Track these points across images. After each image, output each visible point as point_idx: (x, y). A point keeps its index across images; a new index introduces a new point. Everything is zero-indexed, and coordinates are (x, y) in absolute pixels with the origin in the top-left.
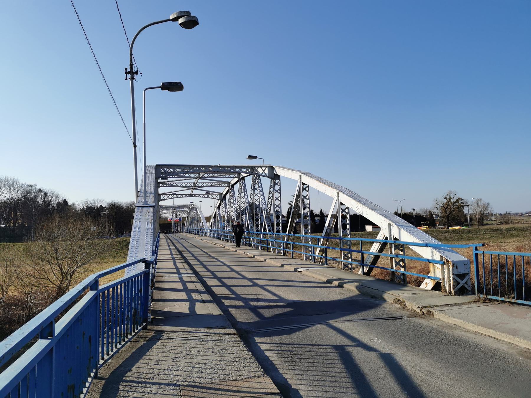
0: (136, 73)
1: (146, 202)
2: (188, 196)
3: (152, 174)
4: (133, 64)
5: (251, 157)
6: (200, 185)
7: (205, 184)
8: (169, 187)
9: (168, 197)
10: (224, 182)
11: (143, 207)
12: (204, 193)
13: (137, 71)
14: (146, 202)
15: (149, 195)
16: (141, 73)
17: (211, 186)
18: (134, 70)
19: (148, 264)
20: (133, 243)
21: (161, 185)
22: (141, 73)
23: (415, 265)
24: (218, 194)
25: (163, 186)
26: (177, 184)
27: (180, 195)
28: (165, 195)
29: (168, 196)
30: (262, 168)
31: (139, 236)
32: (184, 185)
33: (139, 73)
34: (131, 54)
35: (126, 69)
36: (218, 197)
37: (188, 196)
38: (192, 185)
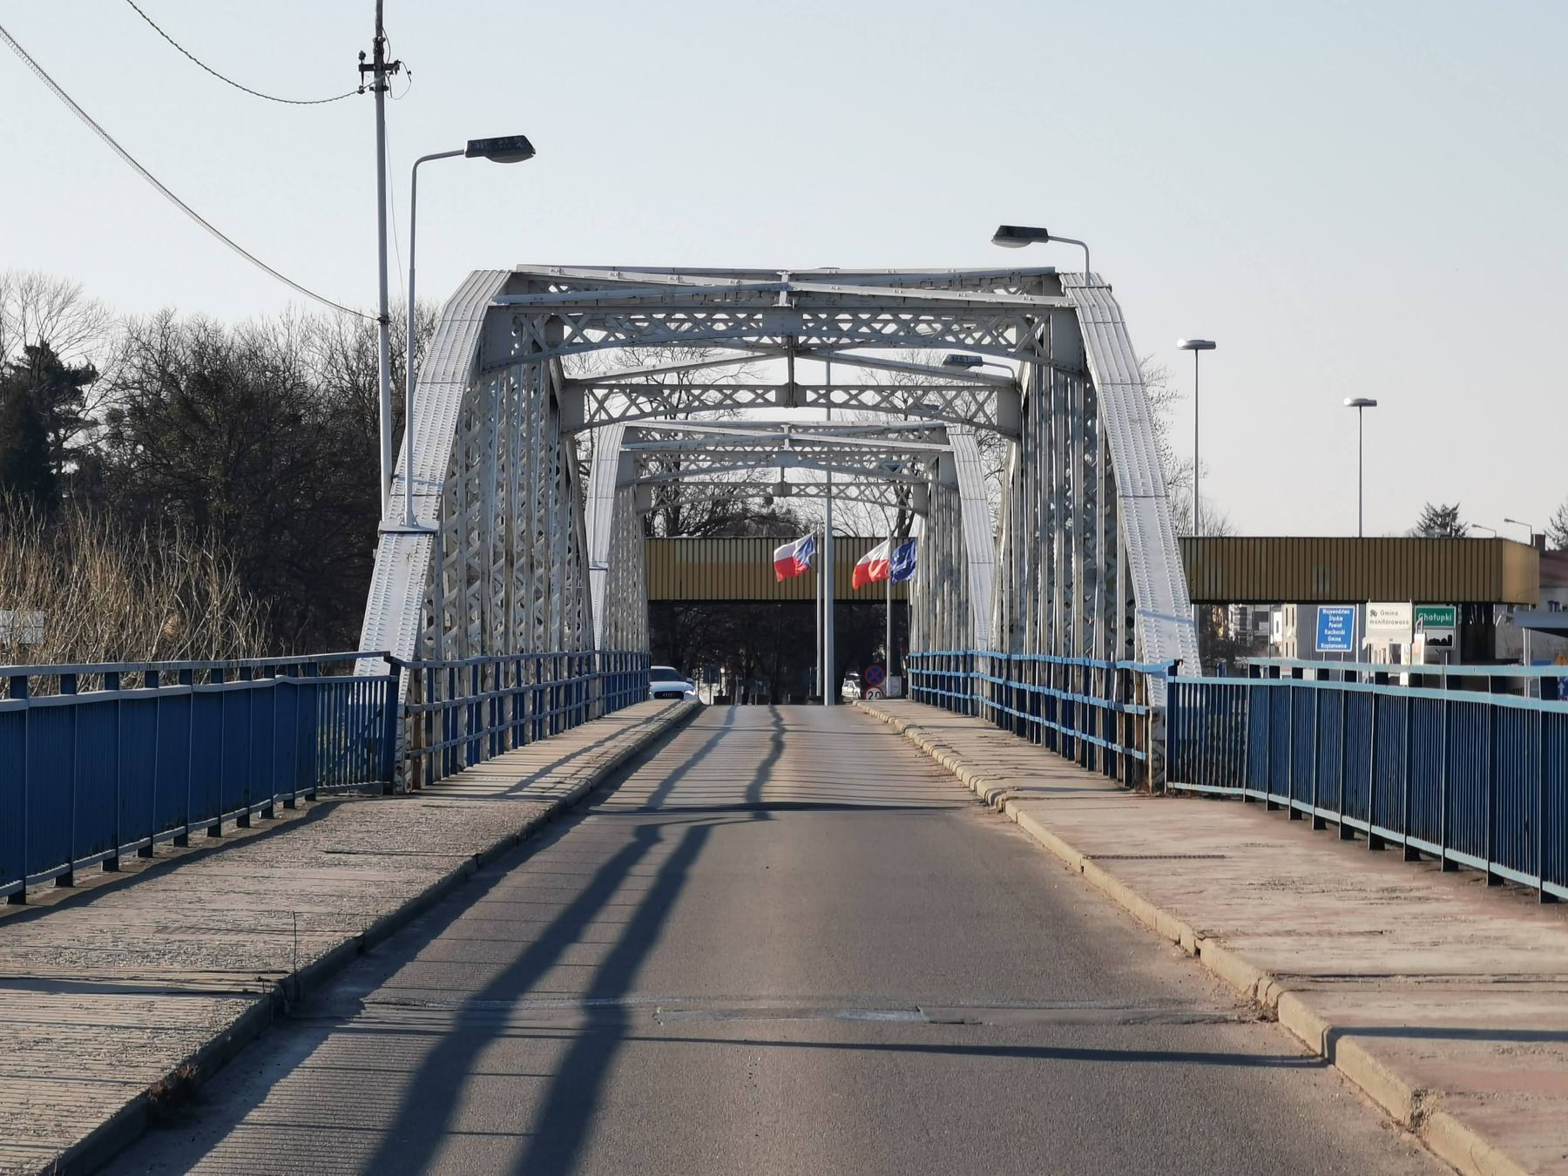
1: (412, 518)
2: (771, 396)
3: (452, 383)
5: (1009, 234)
11: (402, 533)
14: (412, 518)
15: (424, 489)
18: (388, 58)
20: (369, 632)
22: (409, 73)
28: (611, 387)
31: (384, 617)
35: (362, 56)
37: (771, 396)
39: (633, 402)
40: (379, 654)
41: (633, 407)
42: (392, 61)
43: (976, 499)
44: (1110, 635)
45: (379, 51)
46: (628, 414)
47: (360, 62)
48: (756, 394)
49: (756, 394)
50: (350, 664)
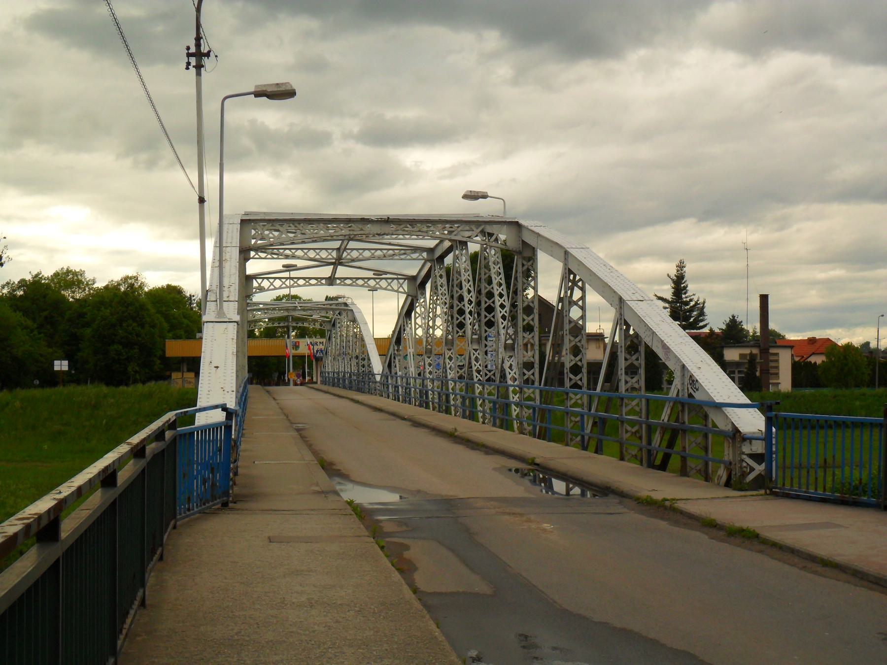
0: (208, 55)
4: (202, 38)
6: (355, 254)
7: (355, 251)
8: (273, 258)
9: (272, 284)
10: (416, 249)
12: (370, 274)
13: (209, 52)
16: (216, 56)
17: (373, 257)
18: (204, 49)
19: (229, 414)
21: (252, 253)
22: (216, 56)
23: (317, 294)
24: (405, 279)
25: (257, 256)
26: (293, 251)
27: (304, 279)
29: (272, 280)
30: (257, 280)
32: (312, 254)
33: (211, 53)
34: (198, 26)
35: (188, 48)
36: (405, 286)
37: (324, 281)
38: (334, 254)
39: (260, 285)
40: (216, 407)
41: (272, 286)
42: (206, 51)
43: (800, 467)
44: (377, 258)
45: (198, 45)
46: (270, 288)
47: (187, 51)
48: (306, 281)
49: (306, 281)
50: (191, 419)
